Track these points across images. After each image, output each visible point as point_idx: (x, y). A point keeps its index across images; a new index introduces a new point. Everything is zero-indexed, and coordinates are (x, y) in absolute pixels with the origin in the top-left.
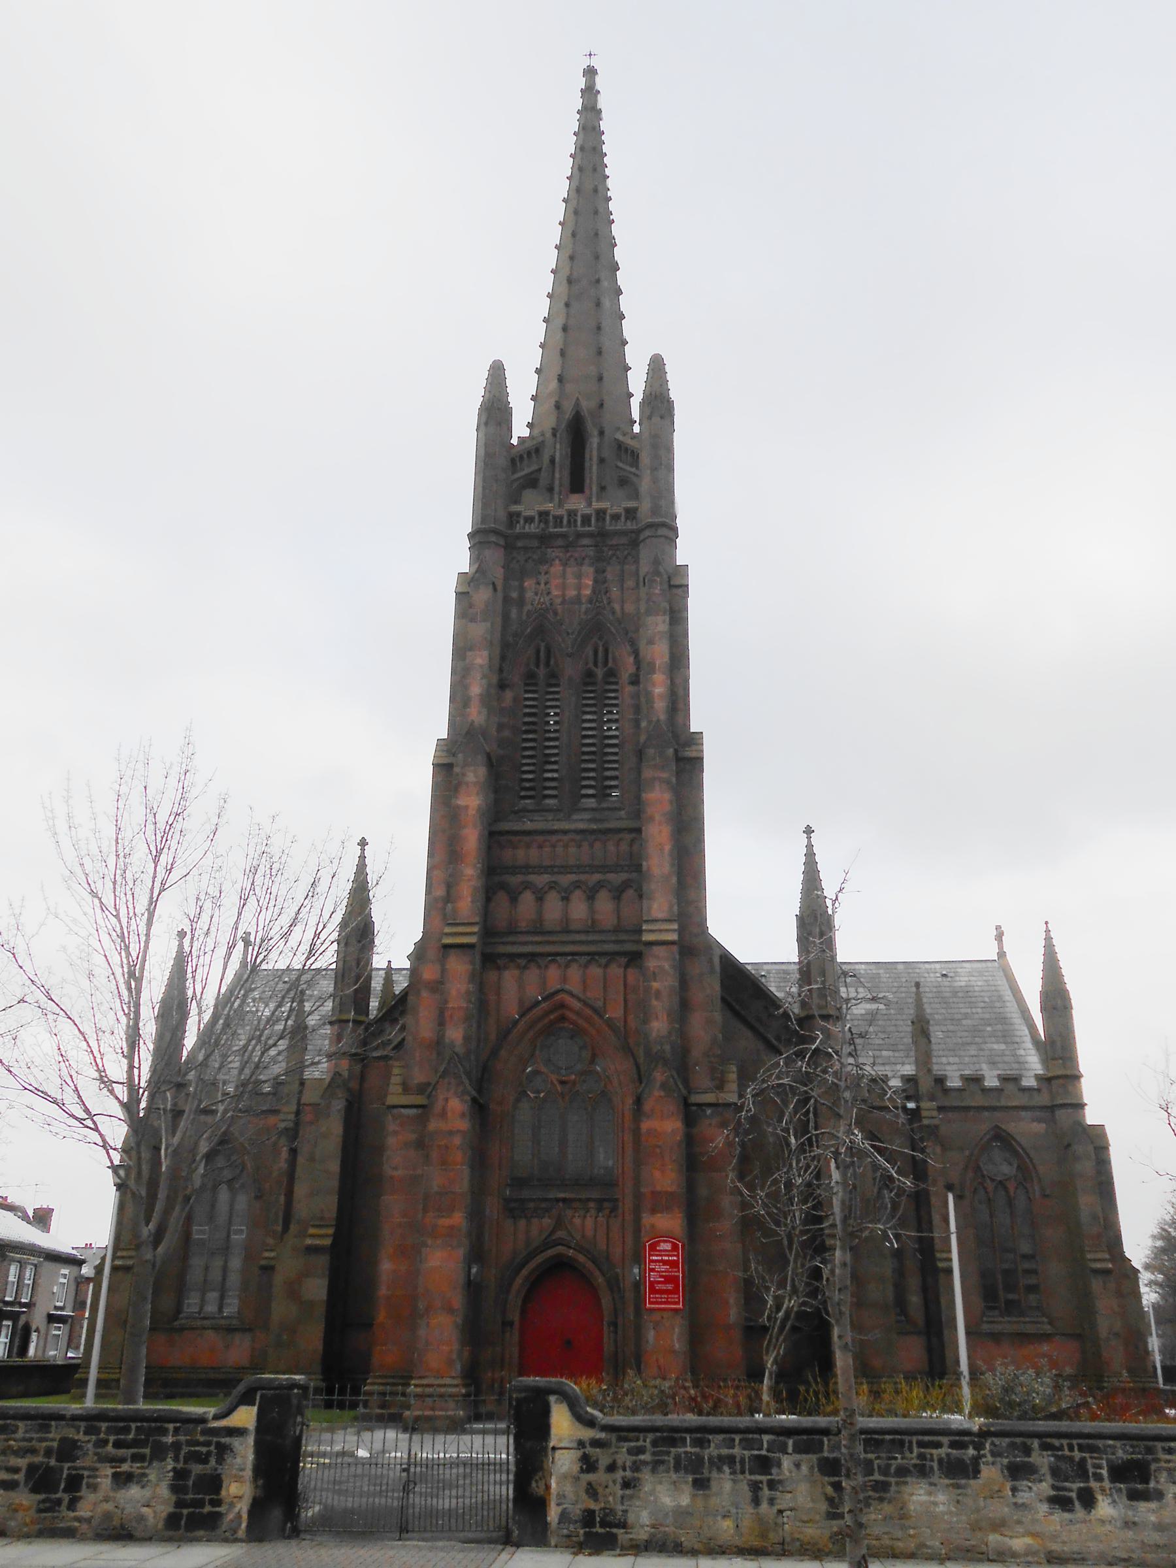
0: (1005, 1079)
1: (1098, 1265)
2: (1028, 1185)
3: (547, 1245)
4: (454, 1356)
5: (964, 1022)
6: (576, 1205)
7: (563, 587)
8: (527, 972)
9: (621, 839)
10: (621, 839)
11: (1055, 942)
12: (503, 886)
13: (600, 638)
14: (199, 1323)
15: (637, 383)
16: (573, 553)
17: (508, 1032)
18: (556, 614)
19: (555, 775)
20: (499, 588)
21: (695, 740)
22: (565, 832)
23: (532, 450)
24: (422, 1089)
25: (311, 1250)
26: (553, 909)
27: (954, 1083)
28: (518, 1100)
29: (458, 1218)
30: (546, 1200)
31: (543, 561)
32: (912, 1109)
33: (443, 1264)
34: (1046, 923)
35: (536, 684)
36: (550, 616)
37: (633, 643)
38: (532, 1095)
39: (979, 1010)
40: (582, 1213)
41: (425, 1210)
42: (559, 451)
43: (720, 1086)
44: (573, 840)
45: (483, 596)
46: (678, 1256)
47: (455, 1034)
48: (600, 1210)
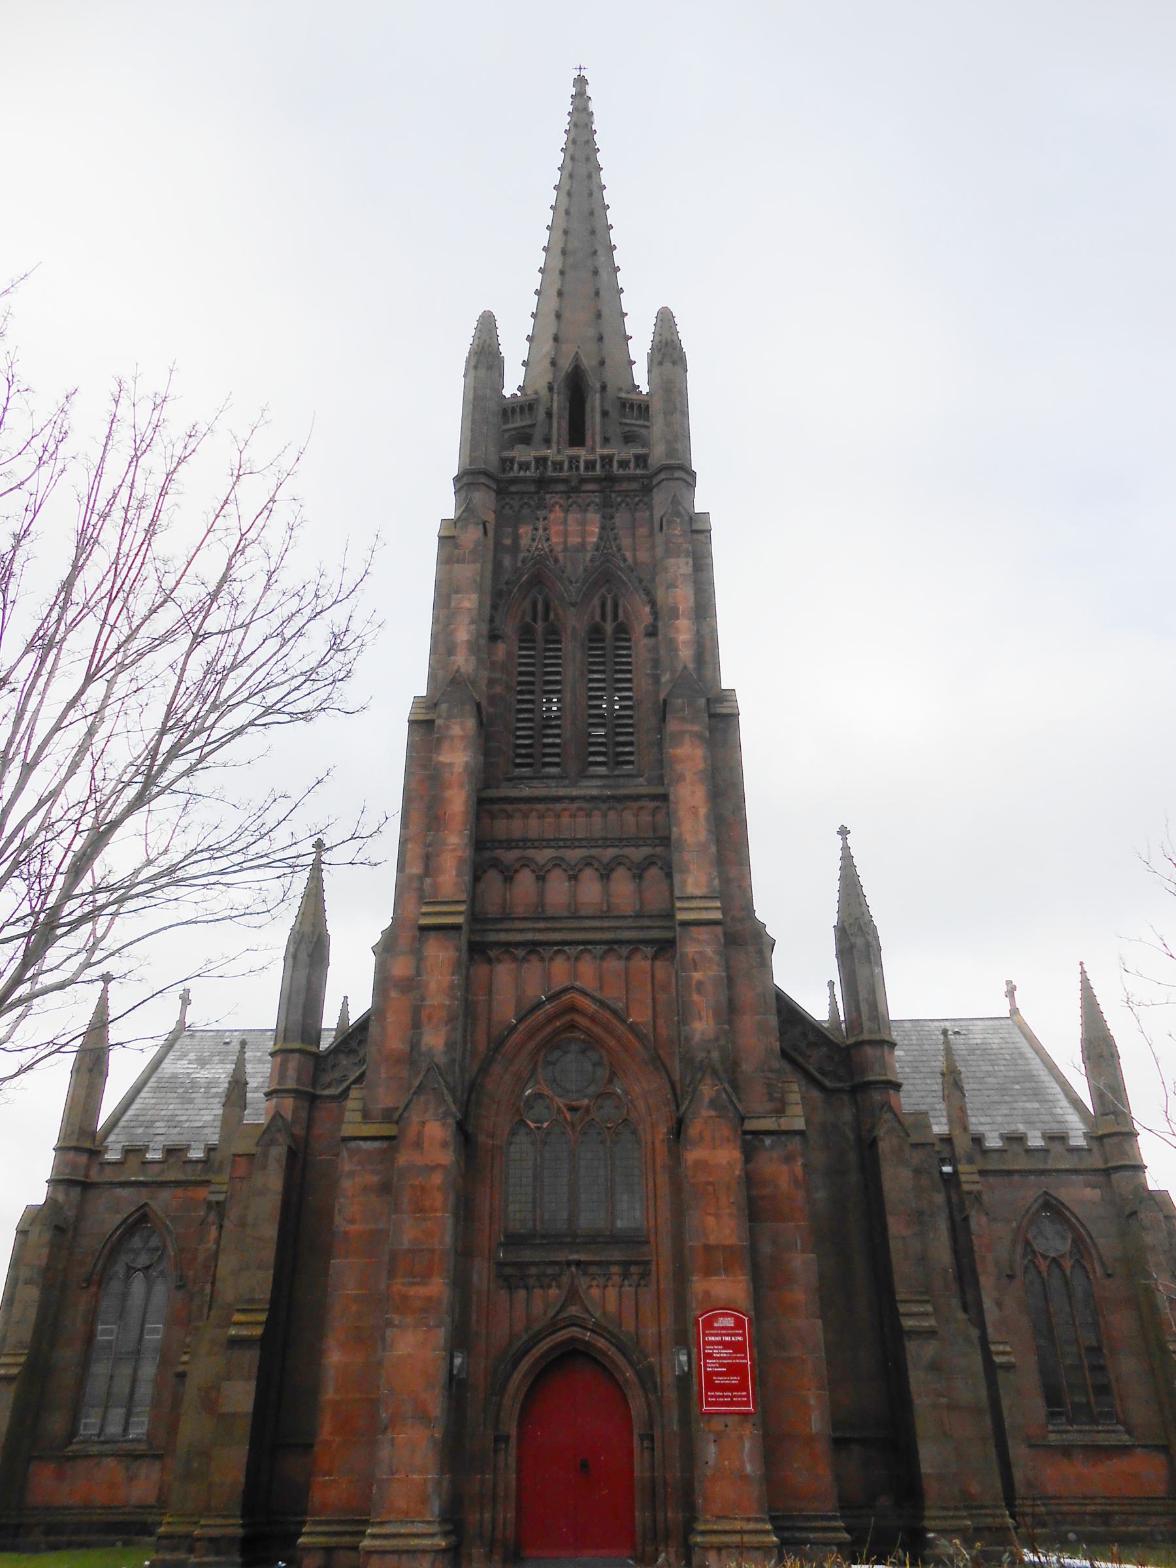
2: (1089, 1267)
3: (554, 1326)
5: (988, 1080)
6: (593, 1269)
7: (566, 534)
9: (641, 808)
10: (641, 808)
11: (1092, 984)
12: (496, 864)
13: (609, 591)
14: (95, 1449)
15: (640, 349)
16: (574, 504)
17: (501, 1042)
18: (556, 560)
19: (557, 741)
20: (491, 528)
21: (728, 697)
22: (573, 799)
23: (524, 406)
24: (388, 1116)
25: (235, 1343)
26: (558, 890)
27: (993, 1142)
28: (513, 1133)
29: (438, 1287)
31: (542, 505)
32: (947, 1174)
33: (415, 1351)
34: (1081, 964)
35: (533, 641)
36: (550, 563)
37: (648, 592)
38: (532, 1125)
39: (1002, 1068)
40: (601, 1281)
41: (392, 1274)
42: (558, 403)
44: (580, 809)
45: (471, 536)
46: (743, 1335)
47: (435, 1040)
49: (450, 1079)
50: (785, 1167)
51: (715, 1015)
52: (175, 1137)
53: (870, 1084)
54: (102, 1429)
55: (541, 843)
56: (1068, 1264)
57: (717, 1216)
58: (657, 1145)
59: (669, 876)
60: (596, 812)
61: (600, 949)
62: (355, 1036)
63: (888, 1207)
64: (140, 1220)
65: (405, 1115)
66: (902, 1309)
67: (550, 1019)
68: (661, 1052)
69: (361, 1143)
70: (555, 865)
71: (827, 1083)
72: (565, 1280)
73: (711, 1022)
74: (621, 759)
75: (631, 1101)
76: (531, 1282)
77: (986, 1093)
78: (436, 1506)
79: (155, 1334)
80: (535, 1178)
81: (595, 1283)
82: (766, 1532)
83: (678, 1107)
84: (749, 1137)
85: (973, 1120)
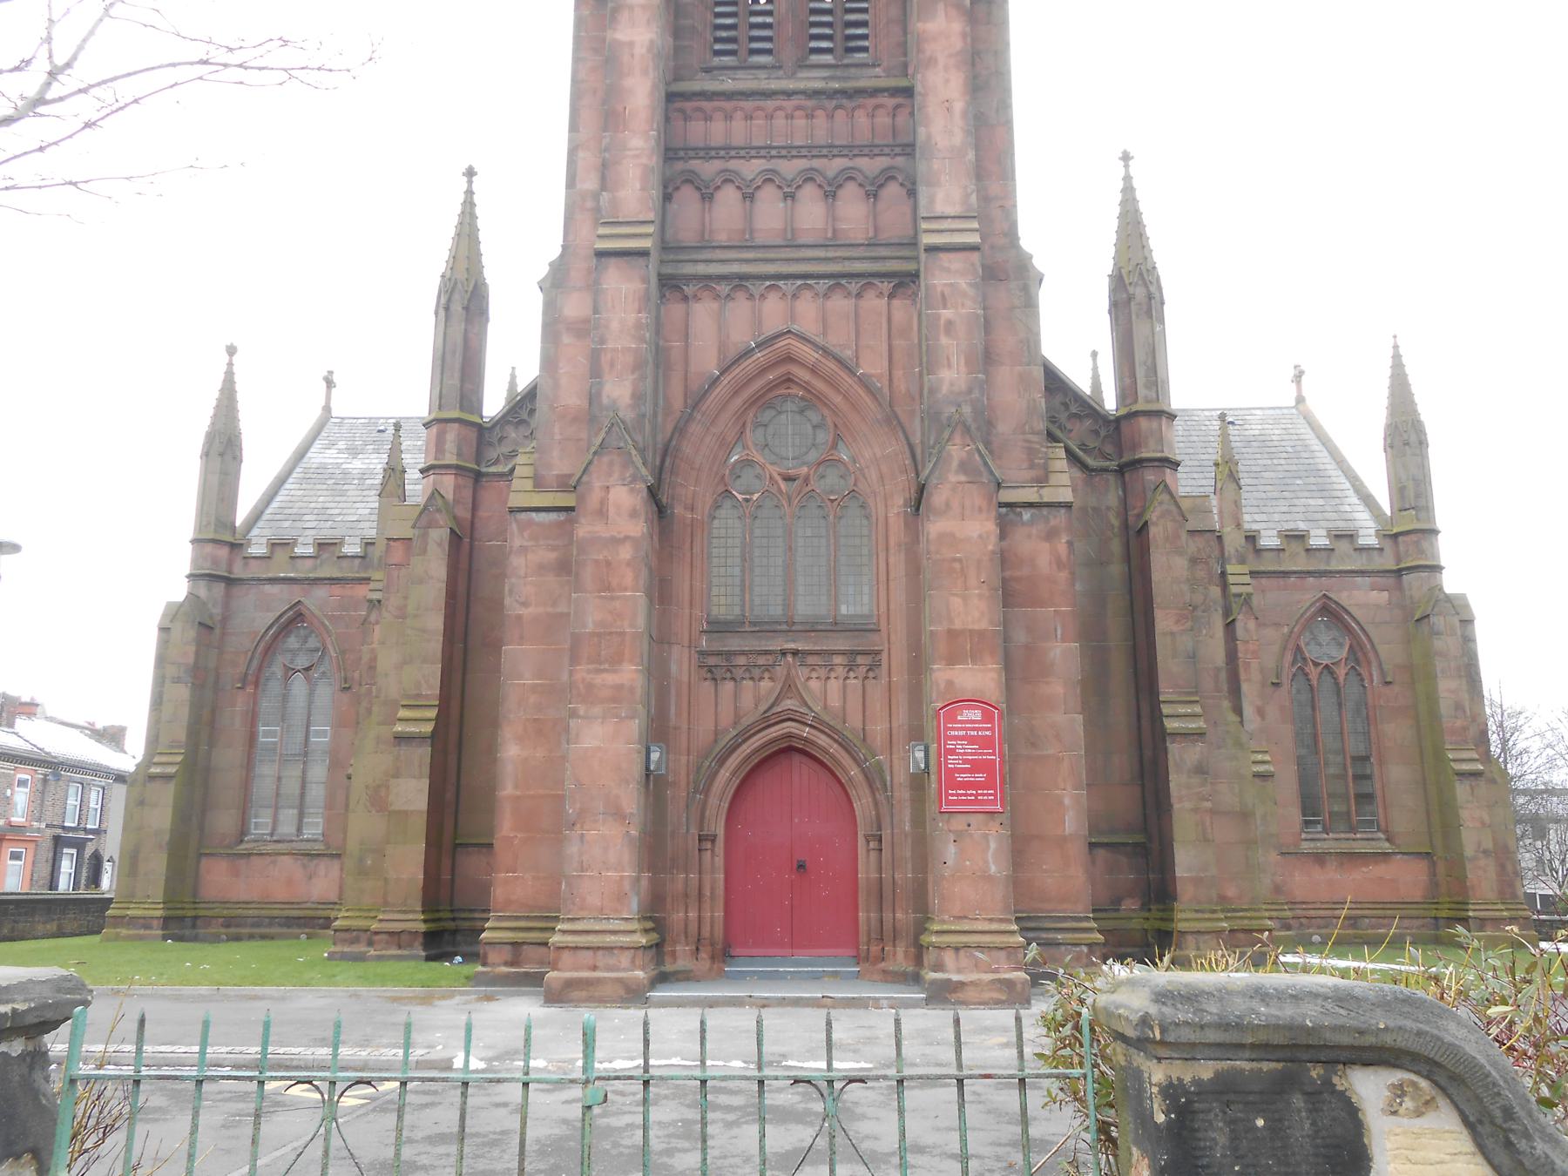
0: (1337, 536)
1: (1465, 767)
2: (1365, 674)
3: (766, 722)
4: (627, 886)
6: (811, 660)
8: (730, 304)
9: (877, 107)
10: (877, 107)
12: (691, 179)
14: (271, 847)
19: (769, 20)
22: (788, 94)
24: (569, 485)
25: (400, 739)
27: (1269, 540)
28: (717, 506)
29: (630, 674)
30: (767, 652)
33: (605, 746)
40: (822, 672)
41: (574, 659)
43: (1042, 481)
44: (798, 108)
47: (619, 391)
48: (851, 667)
49: (639, 438)
50: (1046, 546)
51: (966, 363)
52: (327, 533)
53: (1141, 461)
54: (274, 829)
55: (749, 152)
56: (1341, 672)
57: (965, 598)
58: (892, 520)
59: (912, 193)
60: (819, 113)
61: (823, 285)
62: (523, 405)
63: (1157, 600)
64: (295, 619)
65: (585, 479)
66: (1166, 709)
67: (764, 370)
68: (898, 410)
69: (534, 514)
70: (766, 181)
71: (1090, 461)
72: (780, 671)
73: (963, 369)
74: (853, 44)
75: (861, 470)
76: (739, 673)
77: (1262, 488)
78: (634, 905)
79: (322, 734)
80: (744, 560)
81: (814, 675)
82: (1012, 932)
83: (918, 475)
84: (1004, 510)
85: (1246, 517)
